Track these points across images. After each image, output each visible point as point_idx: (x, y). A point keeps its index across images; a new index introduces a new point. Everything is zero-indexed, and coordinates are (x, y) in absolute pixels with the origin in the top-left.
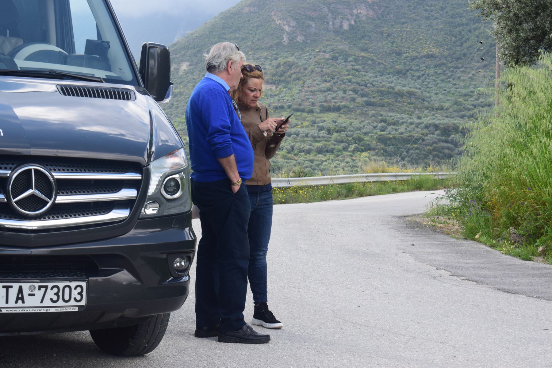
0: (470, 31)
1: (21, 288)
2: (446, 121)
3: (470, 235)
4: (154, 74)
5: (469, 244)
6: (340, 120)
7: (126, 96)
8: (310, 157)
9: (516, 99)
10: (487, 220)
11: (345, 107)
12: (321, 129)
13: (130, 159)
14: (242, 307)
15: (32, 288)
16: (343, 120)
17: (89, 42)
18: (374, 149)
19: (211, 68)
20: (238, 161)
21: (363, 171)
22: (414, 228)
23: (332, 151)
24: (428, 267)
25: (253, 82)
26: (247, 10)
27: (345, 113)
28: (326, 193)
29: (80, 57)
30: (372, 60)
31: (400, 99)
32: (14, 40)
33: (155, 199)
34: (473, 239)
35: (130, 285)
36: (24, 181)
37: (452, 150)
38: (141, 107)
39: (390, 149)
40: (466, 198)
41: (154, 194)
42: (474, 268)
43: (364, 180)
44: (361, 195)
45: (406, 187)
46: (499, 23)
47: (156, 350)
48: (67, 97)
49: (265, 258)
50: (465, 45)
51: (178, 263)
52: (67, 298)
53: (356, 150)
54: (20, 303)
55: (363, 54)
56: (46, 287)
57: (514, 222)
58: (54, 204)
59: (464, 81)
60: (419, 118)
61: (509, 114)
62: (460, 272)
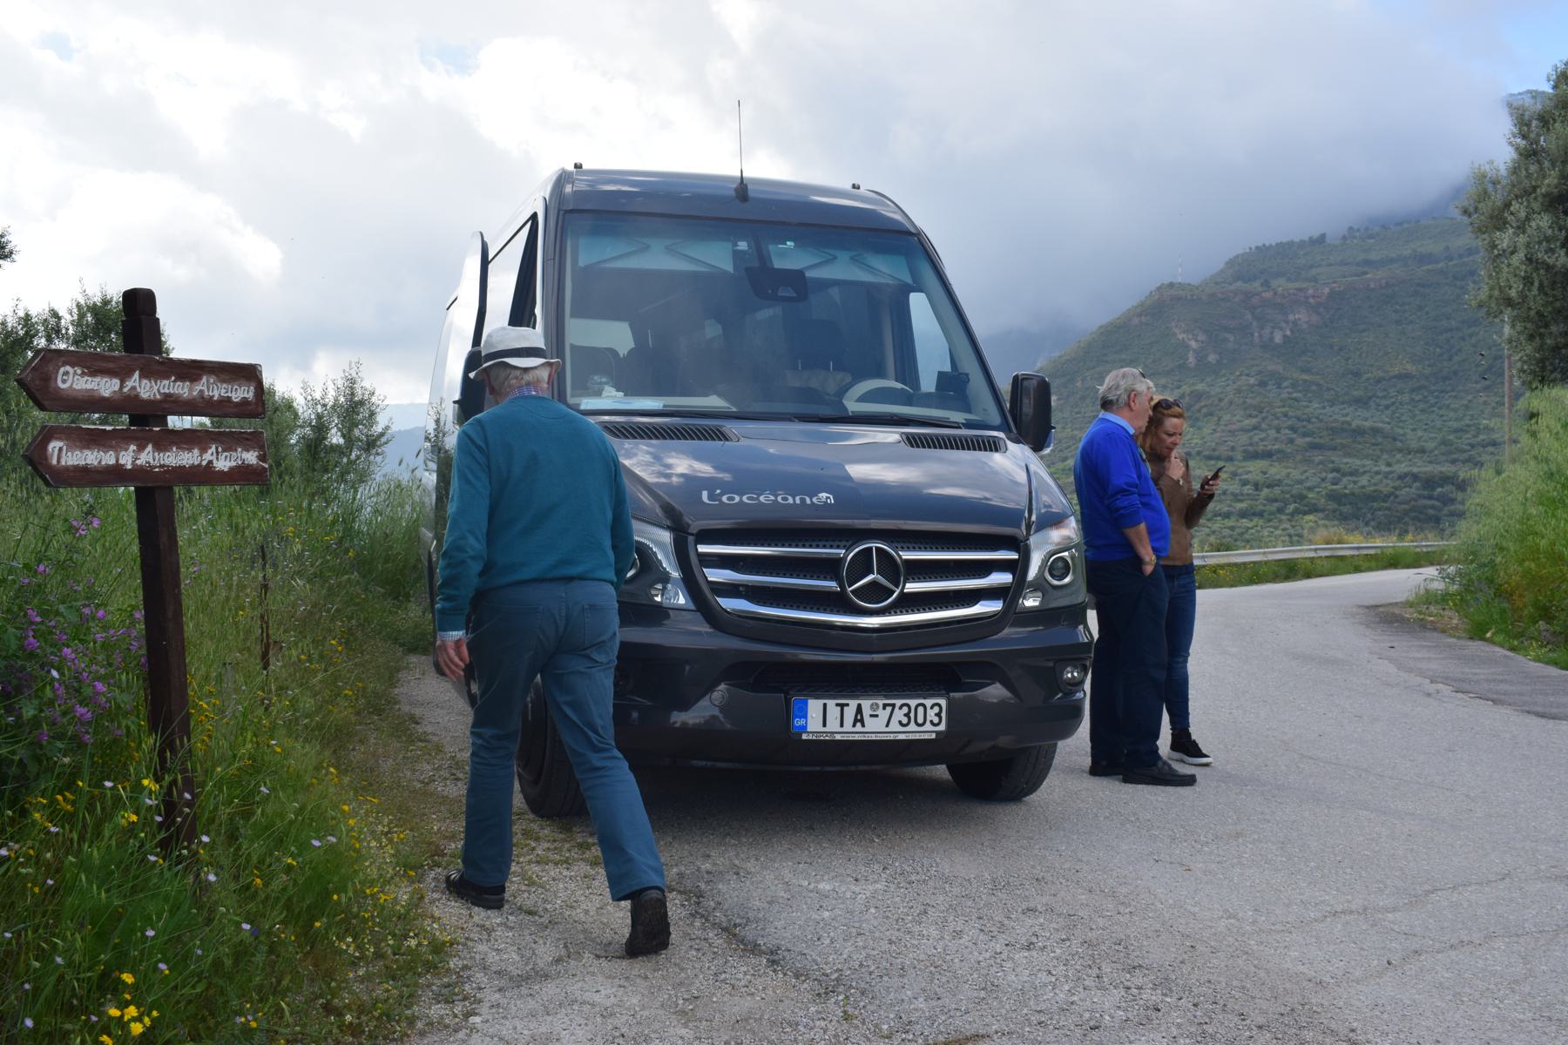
0: (1463, 339)
1: (859, 706)
2: (1429, 468)
3: (1477, 632)
4: (1028, 414)
5: (1476, 647)
6: (1273, 471)
7: (993, 446)
8: (1230, 523)
9: (1544, 435)
10: (1503, 611)
11: (1279, 451)
12: (1245, 483)
13: (1002, 531)
14: (1156, 735)
15: (874, 707)
16: (1276, 470)
17: (941, 375)
18: (1323, 510)
19: (1106, 404)
20: (1151, 532)
21: (1311, 542)
22: (1391, 622)
23: (1261, 515)
24: (1419, 679)
25: (1171, 423)
26: (1136, 321)
27: (1279, 460)
28: (1257, 574)
29: (929, 395)
30: (1318, 385)
31: (1359, 439)
32: (840, 375)
33: (1039, 586)
34: (1483, 639)
35: (1003, 703)
36: (862, 564)
37: (1440, 510)
38: (1013, 462)
39: (1346, 509)
40: (1470, 580)
41: (1036, 578)
42: (1487, 681)
43: (1312, 554)
44: (1308, 576)
45: (1373, 564)
46: (1513, 326)
47: (1038, 793)
48: (916, 450)
49: (1185, 667)
50: (1456, 359)
51: (1070, 674)
52: (920, 720)
53: (1296, 512)
54: (859, 727)
55: (1305, 377)
56: (893, 706)
57: (1546, 614)
58: (902, 594)
59: (1455, 410)
60: (1389, 465)
61: (1536, 458)
62: (1466, 687)
